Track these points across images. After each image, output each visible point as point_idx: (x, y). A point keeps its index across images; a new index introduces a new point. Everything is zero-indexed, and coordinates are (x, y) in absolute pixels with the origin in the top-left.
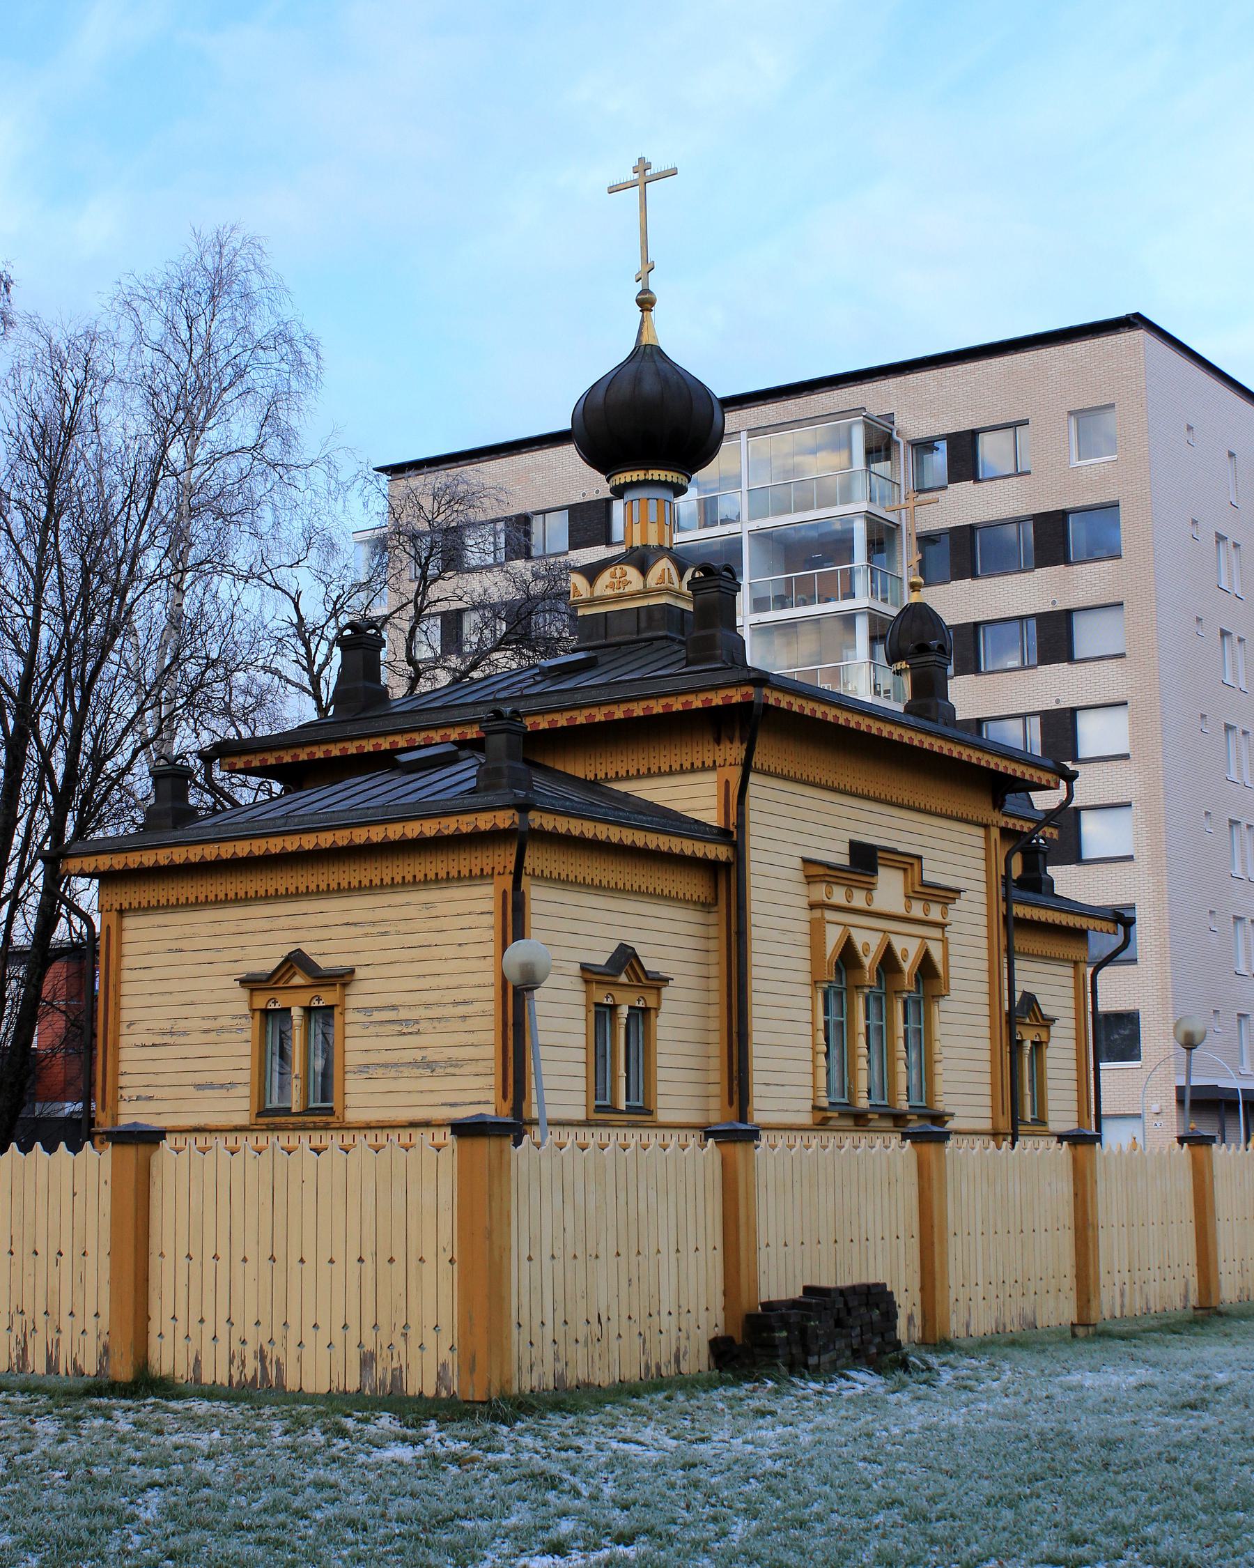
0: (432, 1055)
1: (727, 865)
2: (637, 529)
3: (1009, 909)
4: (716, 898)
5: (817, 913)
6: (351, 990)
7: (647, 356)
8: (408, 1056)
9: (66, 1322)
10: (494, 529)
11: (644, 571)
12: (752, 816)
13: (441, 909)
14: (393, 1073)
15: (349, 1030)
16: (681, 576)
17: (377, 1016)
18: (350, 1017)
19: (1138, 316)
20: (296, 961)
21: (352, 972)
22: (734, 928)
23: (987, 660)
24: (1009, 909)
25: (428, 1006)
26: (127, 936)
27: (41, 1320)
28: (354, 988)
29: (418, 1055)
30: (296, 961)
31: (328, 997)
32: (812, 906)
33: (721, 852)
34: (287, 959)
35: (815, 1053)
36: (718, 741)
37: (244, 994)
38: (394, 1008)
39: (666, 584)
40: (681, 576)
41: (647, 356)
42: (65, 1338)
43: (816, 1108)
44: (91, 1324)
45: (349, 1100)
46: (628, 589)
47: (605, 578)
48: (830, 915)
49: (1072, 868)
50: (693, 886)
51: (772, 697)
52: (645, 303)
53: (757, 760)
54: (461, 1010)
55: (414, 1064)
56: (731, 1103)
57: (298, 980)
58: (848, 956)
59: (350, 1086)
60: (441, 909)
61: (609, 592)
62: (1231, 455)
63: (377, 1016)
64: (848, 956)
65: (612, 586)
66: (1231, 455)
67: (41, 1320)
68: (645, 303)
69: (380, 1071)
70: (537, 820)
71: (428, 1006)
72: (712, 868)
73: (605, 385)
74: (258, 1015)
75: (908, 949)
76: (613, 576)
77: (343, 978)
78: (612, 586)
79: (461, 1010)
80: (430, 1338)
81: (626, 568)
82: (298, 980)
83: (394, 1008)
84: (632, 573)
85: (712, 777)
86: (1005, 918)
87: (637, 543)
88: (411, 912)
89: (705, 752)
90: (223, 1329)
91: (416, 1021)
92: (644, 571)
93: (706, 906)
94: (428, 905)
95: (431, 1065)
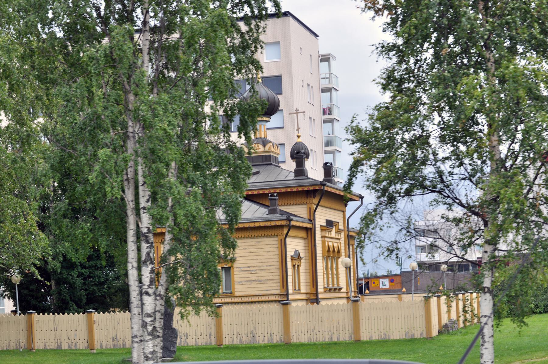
0: (260, 278)
1: (311, 229)
3: (348, 233)
4: (308, 237)
5: (323, 239)
8: (254, 279)
9: (341, 332)
11: (264, 146)
12: (316, 216)
13: (261, 243)
14: (249, 283)
15: (235, 273)
17: (243, 269)
18: (235, 269)
19: (288, 12)
22: (313, 245)
24: (348, 233)
25: (267, 266)
27: (335, 332)
28: (237, 262)
29: (257, 279)
32: (322, 237)
33: (309, 226)
35: (324, 274)
38: (249, 267)
42: (341, 335)
43: (324, 288)
44: (347, 332)
45: (236, 290)
48: (326, 239)
50: (303, 234)
54: (268, 268)
55: (255, 281)
59: (236, 286)
60: (261, 243)
62: (311, 56)
63: (243, 269)
66: (311, 56)
67: (335, 332)
69: (245, 283)
70: (293, 223)
71: (267, 266)
72: (307, 230)
79: (268, 268)
80: (419, 329)
83: (249, 267)
86: (348, 235)
88: (253, 244)
90: (376, 330)
91: (256, 270)
92: (264, 146)
93: (305, 239)
94: (257, 242)
95: (260, 281)
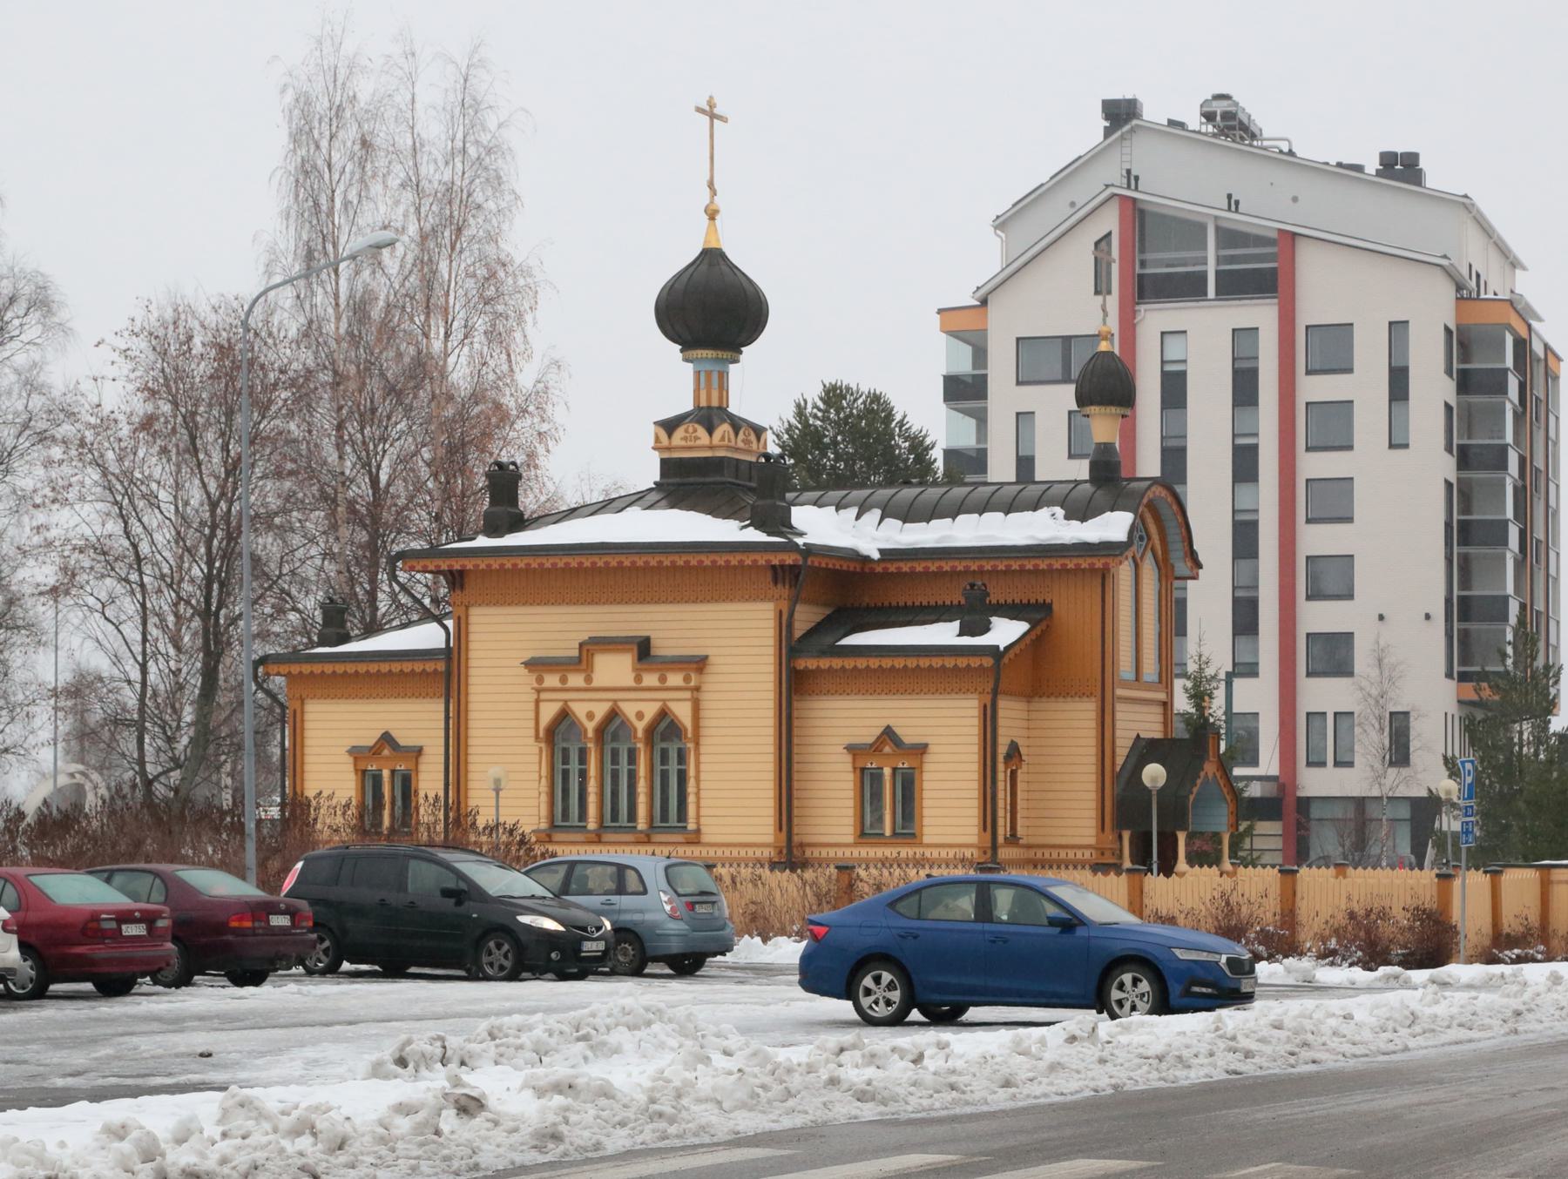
7: (712, 258)
11: (710, 431)
16: (737, 434)
21: (926, 746)
23: (1028, 453)
40: (737, 434)
41: (712, 258)
46: (699, 443)
47: (679, 433)
49: (957, 631)
52: (712, 214)
53: (1002, 686)
56: (985, 829)
61: (683, 443)
65: (685, 439)
68: (712, 214)
75: (640, 712)
77: (921, 750)
78: (685, 439)
84: (701, 431)
87: (703, 403)
92: (710, 431)
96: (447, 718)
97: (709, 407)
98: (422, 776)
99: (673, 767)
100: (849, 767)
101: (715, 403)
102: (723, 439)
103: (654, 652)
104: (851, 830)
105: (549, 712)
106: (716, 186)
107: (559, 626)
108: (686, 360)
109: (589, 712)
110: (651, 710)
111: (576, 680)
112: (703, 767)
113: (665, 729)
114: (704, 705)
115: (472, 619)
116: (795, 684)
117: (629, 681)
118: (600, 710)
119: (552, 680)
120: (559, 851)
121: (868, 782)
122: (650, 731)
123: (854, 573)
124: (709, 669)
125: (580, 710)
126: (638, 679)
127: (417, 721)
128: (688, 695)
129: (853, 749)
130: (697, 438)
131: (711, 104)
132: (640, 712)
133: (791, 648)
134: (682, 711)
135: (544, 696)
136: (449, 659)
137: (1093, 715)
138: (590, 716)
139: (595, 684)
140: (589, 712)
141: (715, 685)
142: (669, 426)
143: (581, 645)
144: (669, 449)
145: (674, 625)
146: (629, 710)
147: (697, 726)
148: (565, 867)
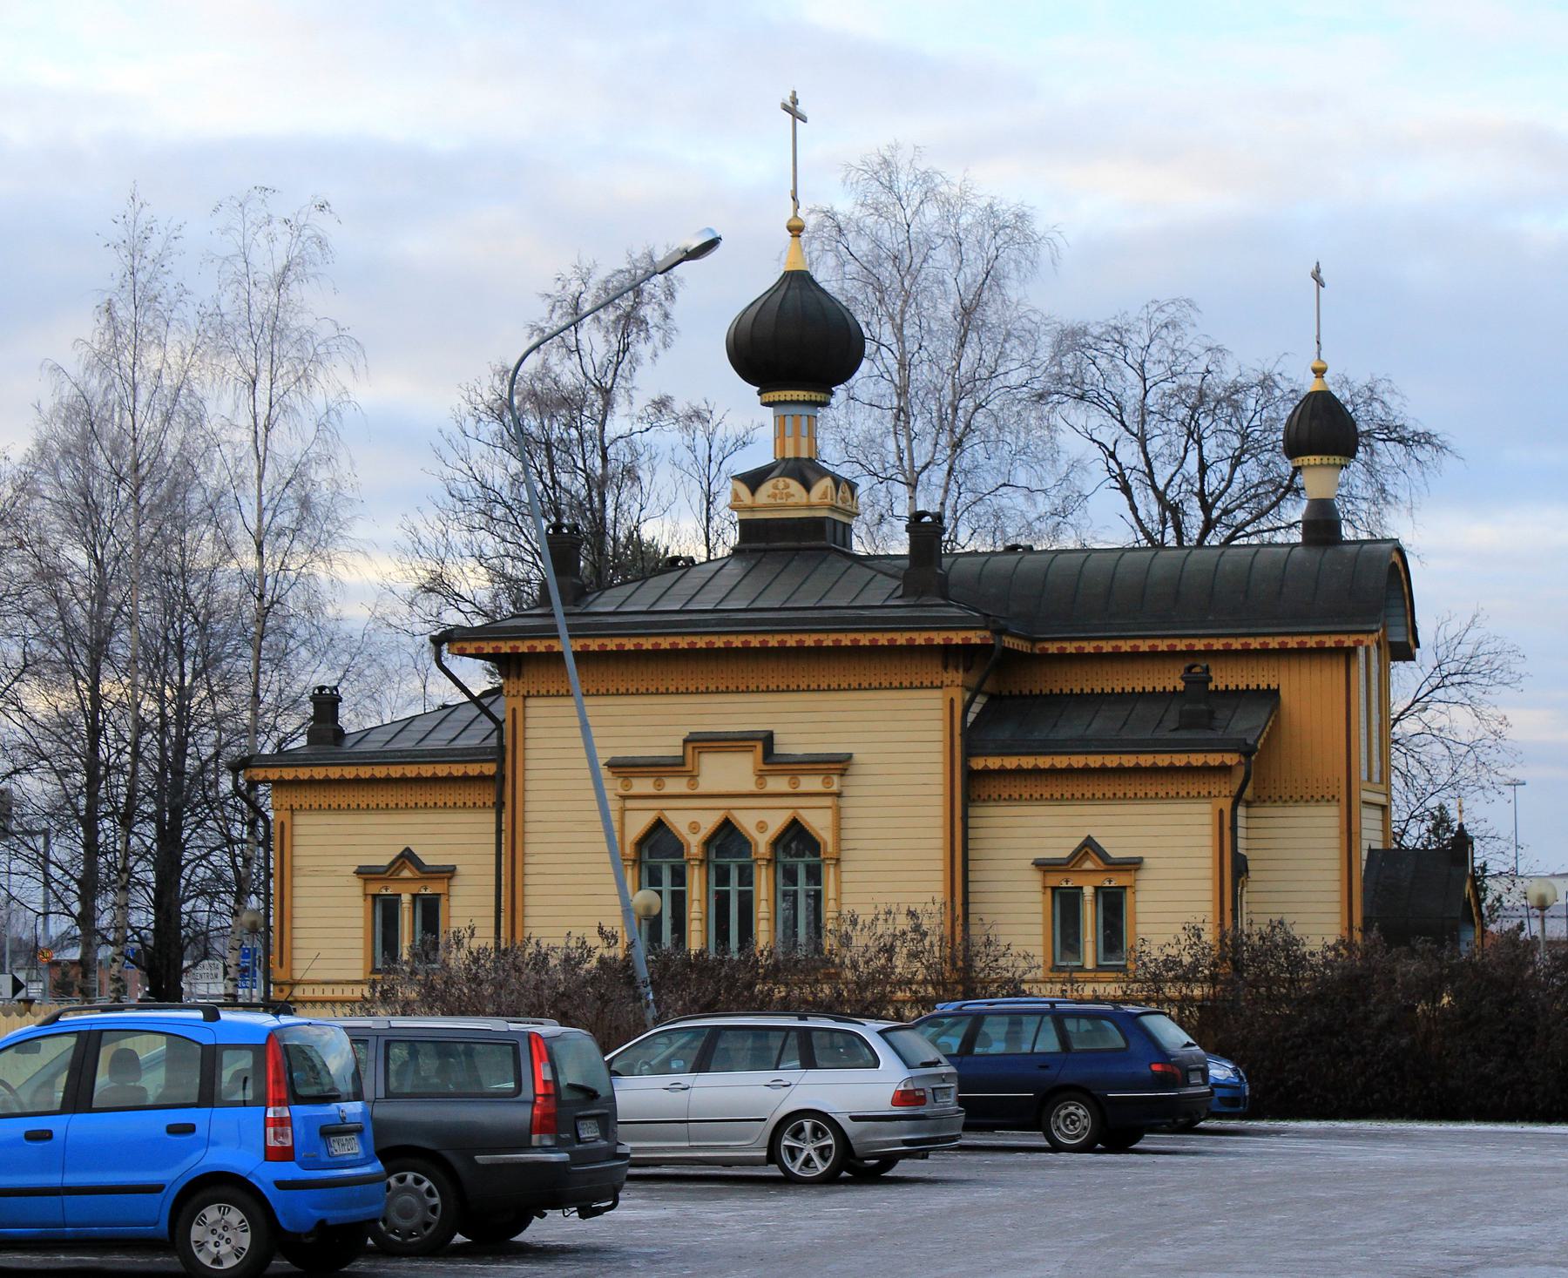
2: (790, 442)
6: (454, 882)
10: (1434, 784)
11: (808, 487)
20: (407, 857)
26: (298, 830)
30: (407, 857)
31: (1118, 880)
34: (401, 856)
36: (945, 668)
37: (1038, 876)
39: (828, 501)
41: (798, 280)
46: (791, 501)
47: (766, 489)
51: (763, 545)
57: (406, 873)
58: (658, 838)
64: (658, 838)
65: (774, 496)
73: (760, 303)
74: (1049, 892)
75: (762, 825)
76: (775, 487)
77: (1133, 865)
81: (788, 480)
82: (406, 873)
84: (795, 487)
85: (938, 693)
87: (790, 454)
89: (934, 672)
92: (808, 487)
96: (499, 831)
97: (797, 459)
98: (454, 901)
99: (734, 887)
100: (1038, 886)
101: (804, 455)
102: (825, 495)
103: (777, 750)
104: (361, 964)
105: (638, 823)
106: (799, 197)
107: (649, 723)
108: (765, 404)
109: (693, 826)
110: (777, 821)
111: (675, 785)
112: (846, 887)
113: (796, 837)
114: (846, 813)
115: (530, 712)
116: (972, 788)
117: (750, 786)
118: (709, 821)
119: (643, 786)
120: (1035, 991)
121: (1066, 904)
122: (779, 843)
123: (1025, 654)
124: (853, 770)
125: (679, 821)
126: (761, 784)
127: (454, 837)
128: (828, 801)
129: (1044, 866)
130: (789, 495)
131: (795, 102)
132: (762, 825)
133: (971, 739)
134: (818, 821)
135: (630, 804)
136: (501, 762)
137: (1335, 822)
138: (695, 827)
139: (699, 790)
140: (693, 826)
141: (861, 791)
142: (753, 480)
143: (686, 741)
144: (751, 509)
145: (804, 720)
146: (747, 821)
147: (839, 839)
148: (969, 1019)
